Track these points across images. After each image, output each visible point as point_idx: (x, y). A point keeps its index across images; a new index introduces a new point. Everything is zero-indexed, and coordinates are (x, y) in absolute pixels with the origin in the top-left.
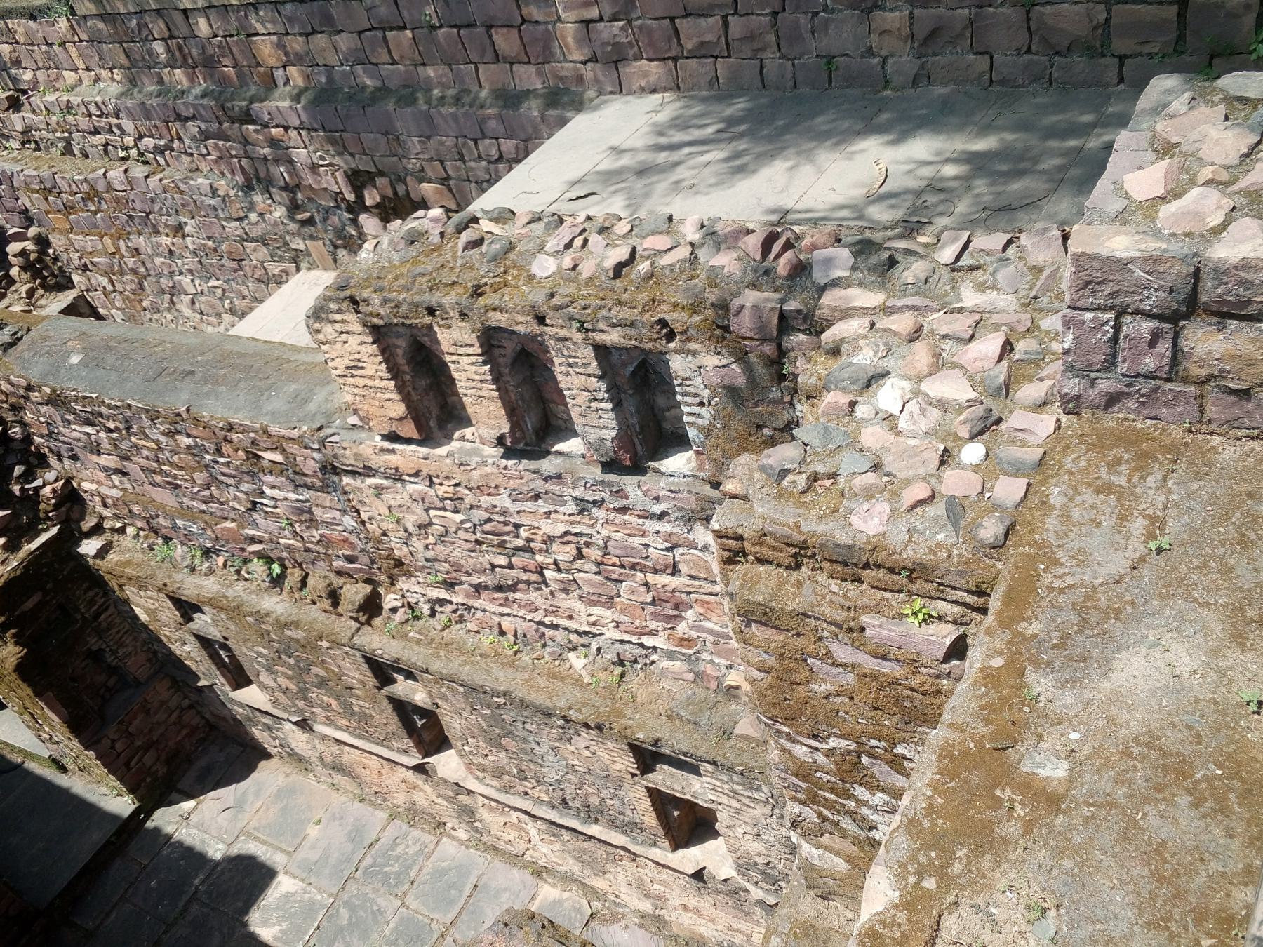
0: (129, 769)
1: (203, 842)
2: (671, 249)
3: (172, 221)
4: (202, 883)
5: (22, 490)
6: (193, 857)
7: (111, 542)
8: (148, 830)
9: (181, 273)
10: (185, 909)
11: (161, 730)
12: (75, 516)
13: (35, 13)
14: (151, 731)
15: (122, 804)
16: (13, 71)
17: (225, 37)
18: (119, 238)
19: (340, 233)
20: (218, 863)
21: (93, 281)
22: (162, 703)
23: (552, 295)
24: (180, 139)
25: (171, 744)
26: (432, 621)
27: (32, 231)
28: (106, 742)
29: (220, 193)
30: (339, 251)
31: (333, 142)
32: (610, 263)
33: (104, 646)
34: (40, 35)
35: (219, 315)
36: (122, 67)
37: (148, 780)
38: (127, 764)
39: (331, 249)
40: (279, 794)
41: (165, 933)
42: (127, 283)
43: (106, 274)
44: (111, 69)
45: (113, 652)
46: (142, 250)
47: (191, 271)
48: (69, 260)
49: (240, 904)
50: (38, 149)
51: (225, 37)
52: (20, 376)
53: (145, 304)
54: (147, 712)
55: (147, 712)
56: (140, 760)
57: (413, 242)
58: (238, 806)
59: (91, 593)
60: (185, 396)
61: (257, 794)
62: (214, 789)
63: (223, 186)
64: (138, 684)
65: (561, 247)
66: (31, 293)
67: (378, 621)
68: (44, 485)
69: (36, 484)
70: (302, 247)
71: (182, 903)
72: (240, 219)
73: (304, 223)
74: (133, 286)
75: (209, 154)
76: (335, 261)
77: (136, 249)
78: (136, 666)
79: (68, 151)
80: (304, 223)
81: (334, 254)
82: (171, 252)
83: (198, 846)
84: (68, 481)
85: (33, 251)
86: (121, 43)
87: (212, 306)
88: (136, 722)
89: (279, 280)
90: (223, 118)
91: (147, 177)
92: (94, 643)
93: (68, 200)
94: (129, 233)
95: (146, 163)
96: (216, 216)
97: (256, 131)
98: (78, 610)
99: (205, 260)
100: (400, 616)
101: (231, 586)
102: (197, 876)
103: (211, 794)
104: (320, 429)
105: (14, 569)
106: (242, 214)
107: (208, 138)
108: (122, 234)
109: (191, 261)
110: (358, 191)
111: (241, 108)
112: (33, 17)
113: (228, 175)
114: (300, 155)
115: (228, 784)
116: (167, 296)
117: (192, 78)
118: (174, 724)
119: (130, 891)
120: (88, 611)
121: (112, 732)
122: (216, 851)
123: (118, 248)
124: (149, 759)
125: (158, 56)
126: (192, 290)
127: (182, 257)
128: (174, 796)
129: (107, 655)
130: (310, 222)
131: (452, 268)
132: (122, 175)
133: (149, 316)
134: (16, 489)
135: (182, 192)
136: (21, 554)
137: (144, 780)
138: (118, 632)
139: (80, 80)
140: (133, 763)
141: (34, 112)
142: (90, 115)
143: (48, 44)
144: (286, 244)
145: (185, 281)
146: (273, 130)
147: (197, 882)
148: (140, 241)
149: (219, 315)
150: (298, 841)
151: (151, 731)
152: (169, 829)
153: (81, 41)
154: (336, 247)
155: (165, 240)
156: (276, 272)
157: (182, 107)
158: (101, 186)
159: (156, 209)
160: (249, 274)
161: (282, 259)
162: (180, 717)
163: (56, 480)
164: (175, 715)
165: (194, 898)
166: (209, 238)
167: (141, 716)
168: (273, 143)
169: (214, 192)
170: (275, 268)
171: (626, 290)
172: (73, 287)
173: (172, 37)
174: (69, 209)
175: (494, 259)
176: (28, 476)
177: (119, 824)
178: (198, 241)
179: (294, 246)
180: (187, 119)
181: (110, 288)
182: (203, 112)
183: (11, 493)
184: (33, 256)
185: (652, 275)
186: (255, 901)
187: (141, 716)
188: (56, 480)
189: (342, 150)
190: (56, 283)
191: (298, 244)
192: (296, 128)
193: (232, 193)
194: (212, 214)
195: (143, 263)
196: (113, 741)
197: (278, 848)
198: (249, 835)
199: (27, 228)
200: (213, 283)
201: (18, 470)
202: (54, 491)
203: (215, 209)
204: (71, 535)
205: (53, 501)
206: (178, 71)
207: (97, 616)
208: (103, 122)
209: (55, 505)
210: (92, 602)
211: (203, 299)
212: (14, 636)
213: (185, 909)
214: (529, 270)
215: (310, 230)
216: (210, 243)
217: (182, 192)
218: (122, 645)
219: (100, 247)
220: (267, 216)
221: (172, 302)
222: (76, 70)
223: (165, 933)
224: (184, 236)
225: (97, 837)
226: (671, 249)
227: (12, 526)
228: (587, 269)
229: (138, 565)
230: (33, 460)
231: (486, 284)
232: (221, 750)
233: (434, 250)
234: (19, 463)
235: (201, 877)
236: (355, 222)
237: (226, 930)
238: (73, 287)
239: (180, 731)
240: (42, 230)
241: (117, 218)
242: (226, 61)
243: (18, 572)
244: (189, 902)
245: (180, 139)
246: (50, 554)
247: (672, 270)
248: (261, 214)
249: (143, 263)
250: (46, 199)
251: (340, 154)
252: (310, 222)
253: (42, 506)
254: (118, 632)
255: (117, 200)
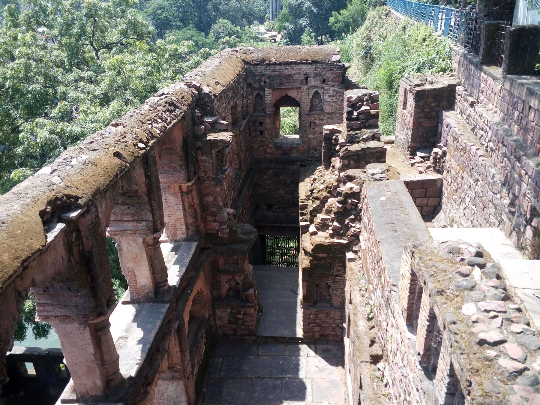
0: (308, 325)
1: (302, 368)
2: (516, 360)
3: (477, 177)
4: (289, 378)
5: (348, 223)
6: (296, 368)
7: (356, 260)
8: (298, 346)
9: (468, 196)
10: (278, 378)
11: (327, 325)
12: (354, 243)
13: (496, 79)
14: (324, 322)
15: (300, 333)
16: (480, 94)
17: (536, 124)
18: (461, 170)
19: (518, 226)
20: (298, 378)
21: (447, 177)
22: (334, 318)
23: (454, 323)
24: (499, 150)
25: (326, 332)
26: (383, 387)
27: (445, 149)
28: (308, 312)
29: (495, 179)
30: (514, 232)
31: (535, 191)
32: (482, 336)
33: (332, 286)
34: (492, 87)
35: (468, 220)
36: (504, 113)
37: (311, 334)
38: (309, 324)
39: (512, 229)
40: (333, 382)
41: (268, 378)
42: (454, 186)
43: (451, 178)
44: (501, 111)
45: (333, 290)
46: (464, 179)
47: (471, 198)
48: (446, 166)
49: (287, 396)
50: (468, 123)
51: (536, 124)
52: (366, 191)
53: (454, 197)
54: (327, 316)
55: (327, 316)
56: (313, 326)
57: (450, 253)
58: (321, 370)
59: (341, 268)
60: (384, 237)
61: (329, 374)
62: (322, 358)
63: (497, 177)
64: (332, 306)
65: (483, 309)
66: (428, 167)
67: (373, 366)
68: (354, 227)
69: (353, 225)
70: (505, 219)
71: (279, 376)
72: (494, 193)
73: (510, 212)
74: (455, 189)
75: (502, 163)
76: (510, 234)
77: (463, 177)
78: (335, 300)
79: (473, 130)
80: (510, 212)
81: (512, 231)
82: (470, 186)
83: (300, 367)
84: (360, 232)
85: (440, 155)
86: (508, 105)
87: (468, 215)
88: (322, 315)
89: (491, 225)
90: (513, 154)
91: (481, 156)
92: (330, 282)
93: (458, 146)
94: (465, 170)
95: (487, 151)
96: (488, 186)
97: (518, 167)
98: (333, 269)
99: (476, 198)
100: (378, 373)
101: (361, 306)
102: (290, 374)
103: (320, 358)
104: (394, 285)
105: (325, 242)
106: (496, 192)
107: (505, 157)
108: (463, 170)
109: (473, 195)
110: (533, 216)
111: (519, 154)
112: (494, 80)
113: (502, 175)
114: (524, 186)
115: (327, 361)
116: (460, 200)
117: (519, 131)
118: (332, 328)
119: (276, 357)
120: (335, 272)
121: (313, 310)
122: (302, 374)
123: (459, 172)
124: (316, 329)
125: (514, 117)
126: (467, 204)
127: (472, 191)
128: (313, 347)
129: (331, 289)
130: (513, 213)
131: (446, 275)
132: (475, 150)
133: (452, 202)
134: (347, 221)
135: (485, 169)
136: (332, 240)
137: (310, 333)
138: (339, 286)
139: (492, 109)
140: (311, 325)
141: (474, 111)
142: (484, 123)
143: (492, 92)
144: (501, 214)
145: (468, 199)
146: (523, 171)
147: (288, 376)
148: (466, 175)
149: (468, 220)
150: (319, 401)
151: (324, 322)
152: (302, 353)
153: (500, 96)
154: (514, 230)
155: (471, 181)
156: (492, 221)
157: (506, 140)
158: (468, 149)
159: (476, 169)
160: (484, 214)
161: (496, 218)
162: (336, 327)
163: (358, 228)
164: (334, 325)
165: (282, 379)
166: (482, 192)
167: (324, 315)
168: (520, 176)
169: (493, 177)
170: (492, 219)
171: (475, 354)
172: (442, 175)
173: (522, 113)
174: (456, 149)
175: (458, 287)
176: (353, 221)
177: (294, 336)
178: (479, 190)
179: (503, 217)
180: (504, 145)
181: (450, 183)
182: (509, 147)
183: (345, 221)
184: (438, 156)
185: (491, 360)
186: (293, 400)
187: (324, 315)
188: (358, 228)
189: (536, 197)
190: (439, 170)
191: (504, 217)
192: (529, 176)
193: (498, 182)
194: (488, 184)
195: (462, 184)
196: (311, 313)
197: (313, 395)
198: (312, 382)
199: (445, 146)
200: (474, 207)
201: (352, 217)
202: (355, 231)
203: (490, 184)
204: (348, 247)
205: (352, 234)
206: (516, 126)
207: (337, 276)
208: (486, 128)
209: (352, 235)
210: (339, 271)
211: (468, 210)
212: (310, 260)
213: (278, 378)
214: (463, 304)
215: (510, 215)
216: (481, 193)
217: (485, 169)
218: (336, 291)
219: (456, 168)
220: (502, 199)
221: (460, 203)
222: (493, 105)
223: (268, 378)
224: (477, 185)
225: (286, 333)
226: (516, 360)
227: (337, 230)
228: (477, 328)
229: (353, 273)
230: (358, 218)
231: (446, 293)
232: (337, 350)
233: (452, 263)
234: (354, 215)
235: (290, 376)
236: (525, 226)
237: (277, 397)
238: (442, 175)
239: (331, 331)
240: (447, 150)
241: (465, 163)
242: (531, 134)
243: (326, 244)
244: (280, 378)
245: (499, 150)
246: (339, 247)
247: (498, 369)
248: (501, 197)
249: (462, 184)
250: (454, 141)
251: (535, 198)
252: (513, 213)
253: (348, 232)
254: (339, 286)
255: (469, 157)
